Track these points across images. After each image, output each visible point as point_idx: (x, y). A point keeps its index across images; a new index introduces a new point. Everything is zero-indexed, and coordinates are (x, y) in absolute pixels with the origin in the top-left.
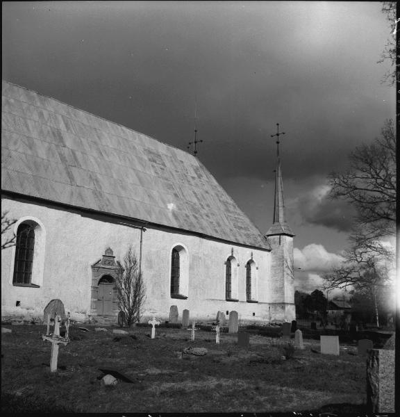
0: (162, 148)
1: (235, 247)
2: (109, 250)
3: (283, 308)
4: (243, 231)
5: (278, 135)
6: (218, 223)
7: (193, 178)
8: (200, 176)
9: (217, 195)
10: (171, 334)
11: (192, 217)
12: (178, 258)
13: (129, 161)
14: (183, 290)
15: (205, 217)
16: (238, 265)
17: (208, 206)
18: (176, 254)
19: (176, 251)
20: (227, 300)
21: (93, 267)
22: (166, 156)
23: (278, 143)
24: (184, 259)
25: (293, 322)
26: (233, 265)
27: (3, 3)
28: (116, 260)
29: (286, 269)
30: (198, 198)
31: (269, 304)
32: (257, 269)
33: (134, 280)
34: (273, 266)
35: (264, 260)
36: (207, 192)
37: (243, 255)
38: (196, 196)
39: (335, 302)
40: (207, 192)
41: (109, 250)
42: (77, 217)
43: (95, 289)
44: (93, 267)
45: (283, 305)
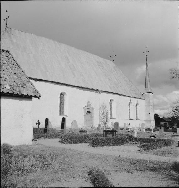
0: (101, 60)
1: (132, 99)
2: (89, 102)
3: (150, 122)
4: (134, 92)
5: (146, 52)
6: (125, 90)
7: (114, 71)
8: (116, 70)
9: (123, 77)
10: (83, 134)
11: (115, 87)
12: (111, 103)
13: (91, 68)
14: (113, 116)
15: (120, 87)
16: (133, 105)
17: (120, 83)
18: (62, 96)
19: (62, 95)
20: (129, 119)
21: (84, 108)
22: (104, 63)
23: (146, 55)
24: (66, 99)
25: (98, 128)
26: (131, 105)
27: (1, 1)
28: (91, 105)
29: (151, 107)
30: (117, 80)
31: (145, 120)
32: (140, 106)
33: (105, 113)
34: (145, 106)
35: (142, 103)
36: (119, 77)
37: (135, 101)
38: (116, 79)
39: (164, 119)
40: (119, 77)
41: (89, 102)
42: (78, 90)
43: (85, 116)
44: (84, 108)
45: (150, 121)
